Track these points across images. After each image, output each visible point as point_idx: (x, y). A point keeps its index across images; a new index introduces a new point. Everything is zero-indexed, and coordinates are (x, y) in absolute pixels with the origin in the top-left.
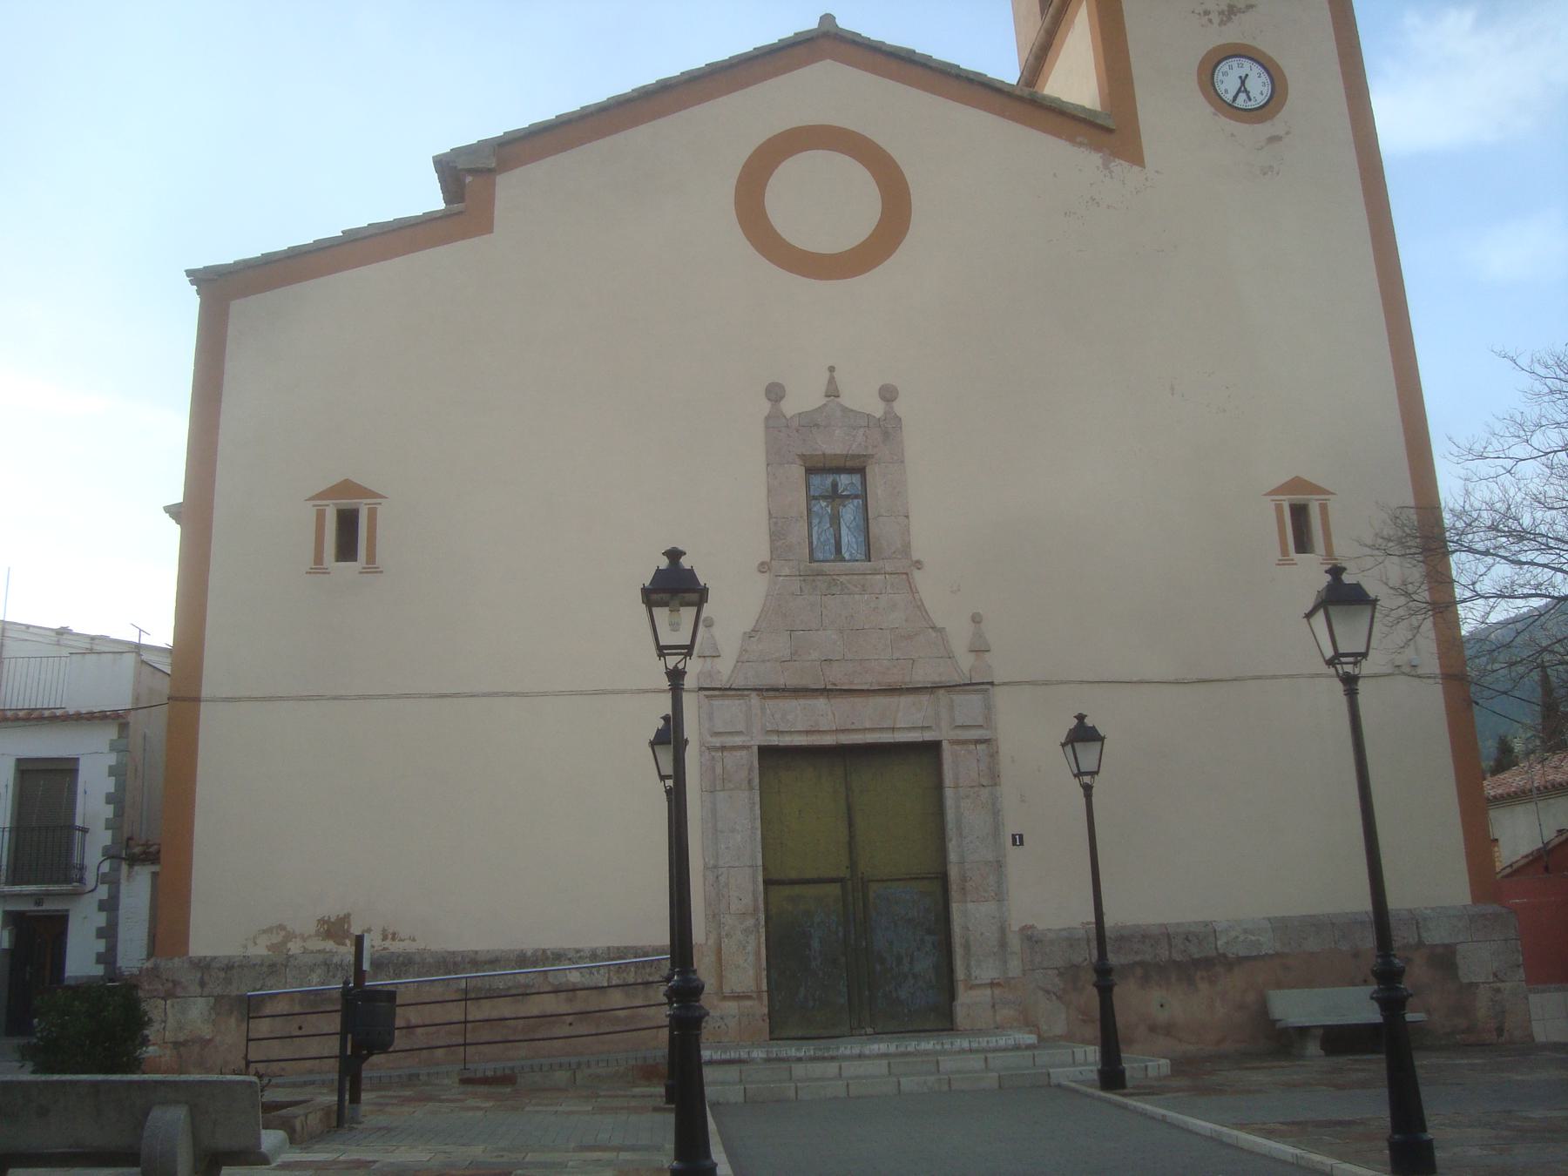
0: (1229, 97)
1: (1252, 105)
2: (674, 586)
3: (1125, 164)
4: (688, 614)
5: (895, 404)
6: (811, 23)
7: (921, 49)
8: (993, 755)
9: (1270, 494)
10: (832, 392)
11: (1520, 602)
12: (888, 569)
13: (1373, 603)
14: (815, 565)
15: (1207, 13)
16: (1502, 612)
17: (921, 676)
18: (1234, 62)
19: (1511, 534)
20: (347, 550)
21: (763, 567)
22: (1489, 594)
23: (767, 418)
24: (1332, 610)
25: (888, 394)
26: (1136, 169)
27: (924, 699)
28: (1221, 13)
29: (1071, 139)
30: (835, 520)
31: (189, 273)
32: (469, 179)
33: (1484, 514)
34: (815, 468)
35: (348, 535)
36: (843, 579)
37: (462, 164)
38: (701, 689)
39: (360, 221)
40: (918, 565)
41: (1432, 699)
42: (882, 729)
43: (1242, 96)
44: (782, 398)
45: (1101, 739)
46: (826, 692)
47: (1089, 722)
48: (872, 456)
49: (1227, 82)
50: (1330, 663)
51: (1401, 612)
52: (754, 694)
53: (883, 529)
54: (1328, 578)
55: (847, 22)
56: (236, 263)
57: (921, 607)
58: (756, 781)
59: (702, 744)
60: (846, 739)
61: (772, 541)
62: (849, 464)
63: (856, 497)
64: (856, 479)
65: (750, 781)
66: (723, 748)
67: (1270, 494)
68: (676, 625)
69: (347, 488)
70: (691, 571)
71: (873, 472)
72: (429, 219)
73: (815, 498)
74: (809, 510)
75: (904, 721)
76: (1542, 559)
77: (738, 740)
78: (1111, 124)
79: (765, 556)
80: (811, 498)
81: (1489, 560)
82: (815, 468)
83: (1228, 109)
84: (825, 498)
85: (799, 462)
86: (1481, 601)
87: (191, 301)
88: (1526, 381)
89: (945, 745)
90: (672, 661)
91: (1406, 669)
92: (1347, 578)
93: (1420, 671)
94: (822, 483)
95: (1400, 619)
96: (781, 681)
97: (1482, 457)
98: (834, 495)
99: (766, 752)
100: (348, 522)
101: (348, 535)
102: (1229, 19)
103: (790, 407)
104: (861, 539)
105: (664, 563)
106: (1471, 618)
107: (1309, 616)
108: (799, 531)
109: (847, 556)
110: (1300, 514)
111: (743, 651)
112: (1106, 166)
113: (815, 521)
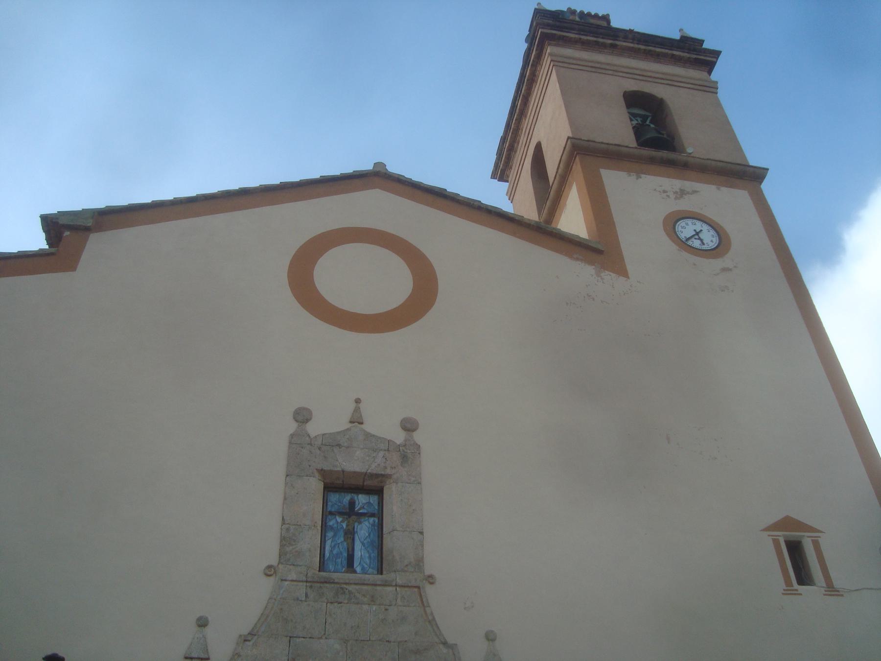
1: (704, 247)
3: (613, 275)
5: (415, 434)
6: (369, 166)
7: (451, 188)
9: (766, 529)
10: (357, 420)
12: (399, 582)
15: (665, 192)
18: (689, 221)
20: (803, 576)
21: (270, 570)
23: (292, 436)
25: (409, 426)
26: (622, 279)
28: (676, 193)
29: (571, 256)
30: (350, 534)
32: (67, 233)
34: (335, 484)
36: (351, 588)
37: (63, 221)
40: (431, 580)
44: (307, 421)
48: (389, 476)
53: (396, 543)
61: (282, 546)
62: (368, 483)
63: (373, 515)
64: (374, 499)
67: (766, 529)
69: (787, 523)
71: (391, 493)
73: (331, 513)
78: (600, 247)
79: (274, 561)
80: (326, 514)
82: (335, 484)
83: (684, 245)
84: (341, 514)
85: (317, 474)
98: (350, 512)
102: (681, 196)
103: (314, 429)
104: (374, 554)
108: (310, 541)
109: (358, 569)
110: (795, 549)
113: (330, 534)
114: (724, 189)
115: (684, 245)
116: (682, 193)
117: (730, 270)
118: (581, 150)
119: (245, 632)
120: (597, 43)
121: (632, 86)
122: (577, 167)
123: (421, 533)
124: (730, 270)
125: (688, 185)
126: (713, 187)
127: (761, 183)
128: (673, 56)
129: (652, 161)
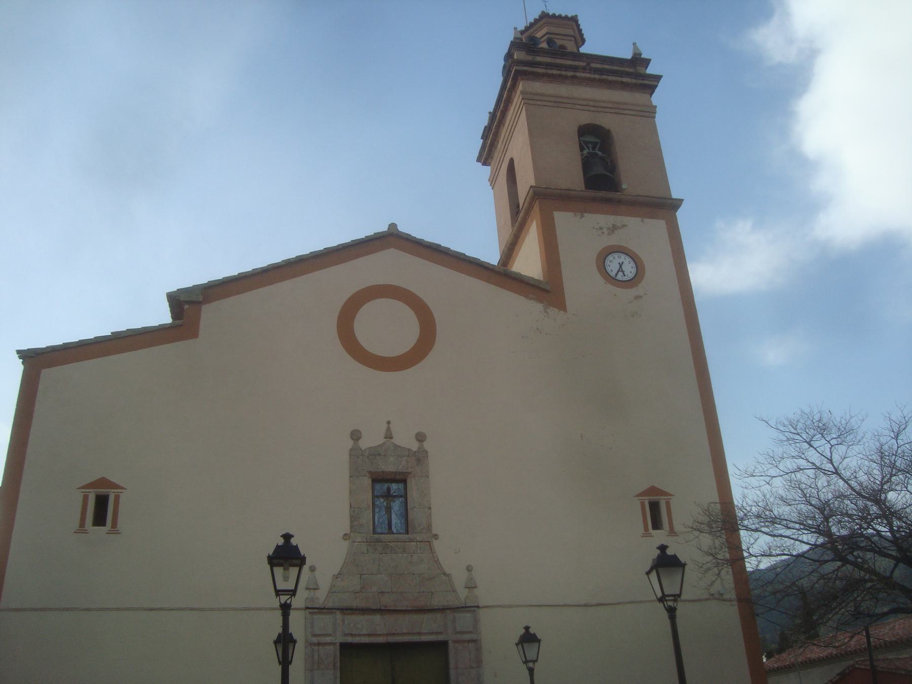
0: (613, 274)
1: (625, 279)
2: (286, 555)
4: (294, 571)
6: (384, 228)
7: (444, 243)
8: (479, 650)
10: (389, 436)
11: (773, 559)
12: (418, 539)
13: (683, 566)
14: (376, 536)
15: (601, 228)
16: (765, 564)
17: (436, 602)
18: (616, 255)
19: (768, 520)
20: (100, 519)
21: (346, 537)
22: (760, 551)
23: (351, 450)
24: (660, 570)
27: (439, 615)
28: (609, 229)
29: (527, 296)
30: (389, 510)
31: (19, 352)
32: (186, 307)
33: (754, 509)
34: (378, 479)
35: (101, 510)
36: (392, 544)
38: (307, 608)
39: (122, 327)
40: (436, 536)
41: (731, 613)
42: (413, 634)
43: (620, 274)
44: (360, 438)
45: (539, 641)
46: (381, 611)
47: (532, 631)
48: (409, 473)
49: (612, 264)
50: (662, 600)
51: (709, 565)
52: (338, 612)
53: (416, 515)
54: (658, 552)
55: (404, 228)
56: (47, 348)
57: (437, 561)
58: (338, 664)
59: (306, 641)
60: (391, 639)
61: (351, 522)
62: (398, 477)
63: (401, 496)
64: (401, 486)
65: (334, 665)
66: (319, 644)
68: (286, 578)
69: (103, 482)
70: (297, 547)
71: (412, 484)
72: (162, 329)
73: (377, 497)
74: (373, 504)
75: (426, 629)
76: (788, 532)
77: (328, 639)
78: (548, 288)
79: (348, 531)
80: (375, 497)
81: (756, 534)
82: (378, 479)
83: (612, 280)
84: (383, 497)
86: (754, 558)
87: (18, 368)
88: (775, 434)
89: (450, 642)
90: (284, 598)
91: (717, 596)
92: (669, 552)
93: (725, 597)
94: (382, 488)
95: (709, 569)
96: (355, 604)
97: (752, 476)
98: (388, 495)
99: (344, 647)
100: (102, 503)
101: (101, 510)
102: (613, 232)
103: (364, 444)
104: (403, 521)
105: (281, 541)
106: (750, 565)
107: (648, 573)
109: (394, 531)
110: (655, 507)
111: (333, 586)
112: (546, 311)
113: (377, 510)
114: (646, 220)
115: (612, 280)
116: (614, 228)
117: (641, 297)
118: (540, 195)
119: (336, 573)
120: (560, 76)
121: (585, 118)
122: (536, 208)
123: (430, 508)
124: (641, 297)
125: (619, 220)
126: (639, 219)
127: (651, 94)
128: (622, 83)
129: (594, 199)
